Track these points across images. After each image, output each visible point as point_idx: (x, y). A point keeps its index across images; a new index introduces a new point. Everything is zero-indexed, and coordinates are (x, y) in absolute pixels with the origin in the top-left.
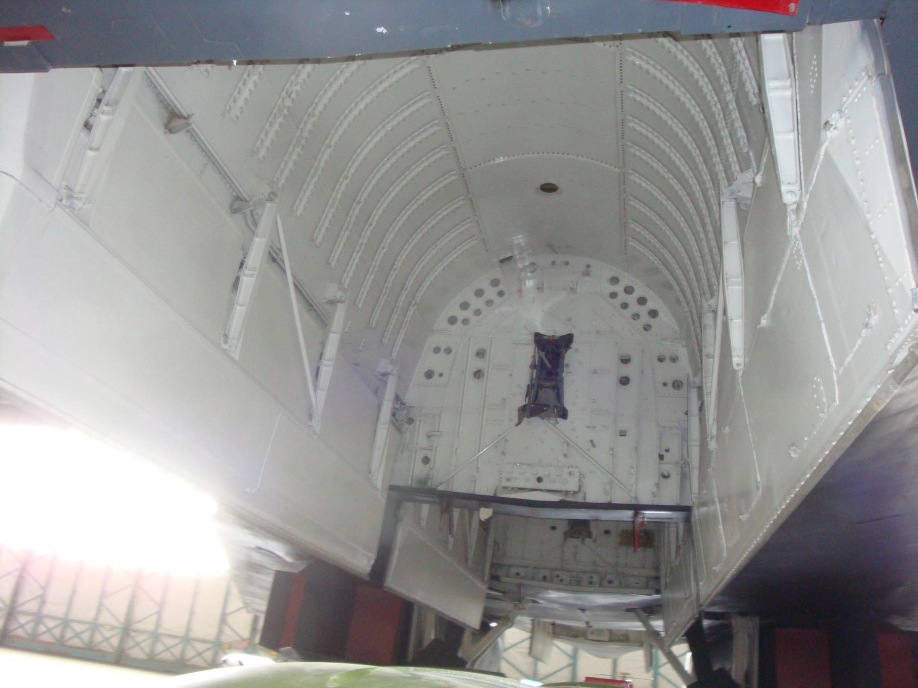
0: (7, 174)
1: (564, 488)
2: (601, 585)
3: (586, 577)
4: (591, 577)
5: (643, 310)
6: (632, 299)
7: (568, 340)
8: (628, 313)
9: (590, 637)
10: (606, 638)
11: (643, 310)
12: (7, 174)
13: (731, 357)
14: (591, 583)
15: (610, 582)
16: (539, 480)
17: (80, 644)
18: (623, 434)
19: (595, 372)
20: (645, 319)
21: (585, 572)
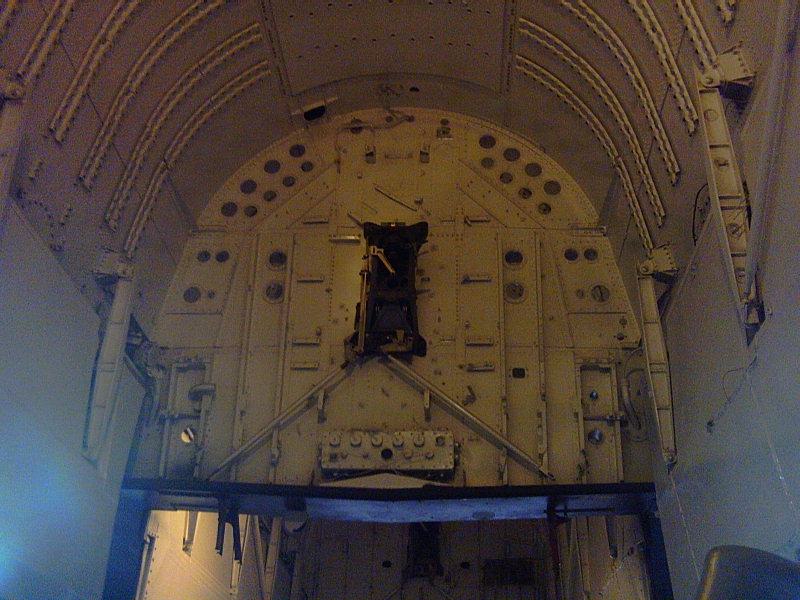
1: (429, 465)
5: (536, 184)
6: (516, 169)
11: (536, 184)
16: (387, 454)
18: (519, 373)
19: (466, 281)
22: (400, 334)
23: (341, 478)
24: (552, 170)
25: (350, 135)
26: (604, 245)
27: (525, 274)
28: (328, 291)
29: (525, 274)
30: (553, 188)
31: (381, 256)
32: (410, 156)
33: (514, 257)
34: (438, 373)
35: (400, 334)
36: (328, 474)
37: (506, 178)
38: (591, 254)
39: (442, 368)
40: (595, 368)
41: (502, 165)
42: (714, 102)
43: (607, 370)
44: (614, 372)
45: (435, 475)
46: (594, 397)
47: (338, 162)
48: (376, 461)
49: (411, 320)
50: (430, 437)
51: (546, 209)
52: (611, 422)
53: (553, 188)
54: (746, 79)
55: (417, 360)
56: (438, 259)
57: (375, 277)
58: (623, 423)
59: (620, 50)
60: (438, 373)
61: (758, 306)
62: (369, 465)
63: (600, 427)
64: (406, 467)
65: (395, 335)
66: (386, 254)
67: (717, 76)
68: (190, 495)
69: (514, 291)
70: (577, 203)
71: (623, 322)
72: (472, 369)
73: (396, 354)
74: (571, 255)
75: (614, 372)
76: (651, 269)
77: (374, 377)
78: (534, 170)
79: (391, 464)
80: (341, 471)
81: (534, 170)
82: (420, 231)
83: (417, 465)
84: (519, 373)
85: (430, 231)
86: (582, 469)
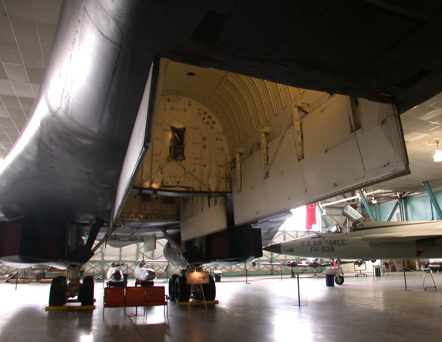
0: (362, 160)
1: (187, 186)
2: (156, 219)
3: (150, 216)
4: (152, 216)
5: (210, 121)
6: (206, 117)
7: (184, 129)
8: (205, 121)
9: (121, 239)
10: (128, 239)
11: (210, 121)
12: (362, 160)
13: (428, 191)
14: (152, 218)
15: (159, 217)
16: (178, 183)
17: (240, 270)
18: (205, 166)
19: (195, 143)
20: (211, 124)
21: (150, 214)
22: (181, 155)
23: (168, 187)
24: (214, 118)
25: (168, 102)
26: (224, 138)
27: (207, 143)
28: (163, 142)
29: (207, 143)
30: (214, 123)
31: (177, 136)
32: (182, 110)
33: (205, 139)
34: (187, 164)
35: (181, 155)
36: (165, 186)
37: (208, 123)
38: (221, 140)
39: (188, 163)
40: (221, 166)
41: (207, 120)
42: (263, 135)
43: (223, 167)
44: (225, 168)
45: (187, 188)
46: (220, 173)
47: (165, 109)
48: (175, 184)
49: (183, 153)
50: (187, 180)
51: (212, 128)
52: (223, 178)
53: (214, 123)
54: (269, 132)
55: (183, 161)
56: (188, 138)
57: (174, 140)
58: (226, 179)
59: (238, 103)
60: (187, 164)
61: (267, 173)
62: (174, 185)
63: (221, 179)
64: (182, 186)
65: (180, 156)
66: (178, 136)
67: (264, 130)
68: (136, 190)
69: (205, 147)
70: (218, 127)
71: (227, 156)
72: (195, 164)
73: (180, 160)
74: (217, 139)
75: (225, 168)
76: (239, 151)
77: (174, 164)
78: (210, 117)
79: (179, 185)
80: (167, 186)
81: (210, 117)
82: (184, 129)
83: (184, 185)
84: (205, 166)
85: (186, 130)
86: (217, 188)
